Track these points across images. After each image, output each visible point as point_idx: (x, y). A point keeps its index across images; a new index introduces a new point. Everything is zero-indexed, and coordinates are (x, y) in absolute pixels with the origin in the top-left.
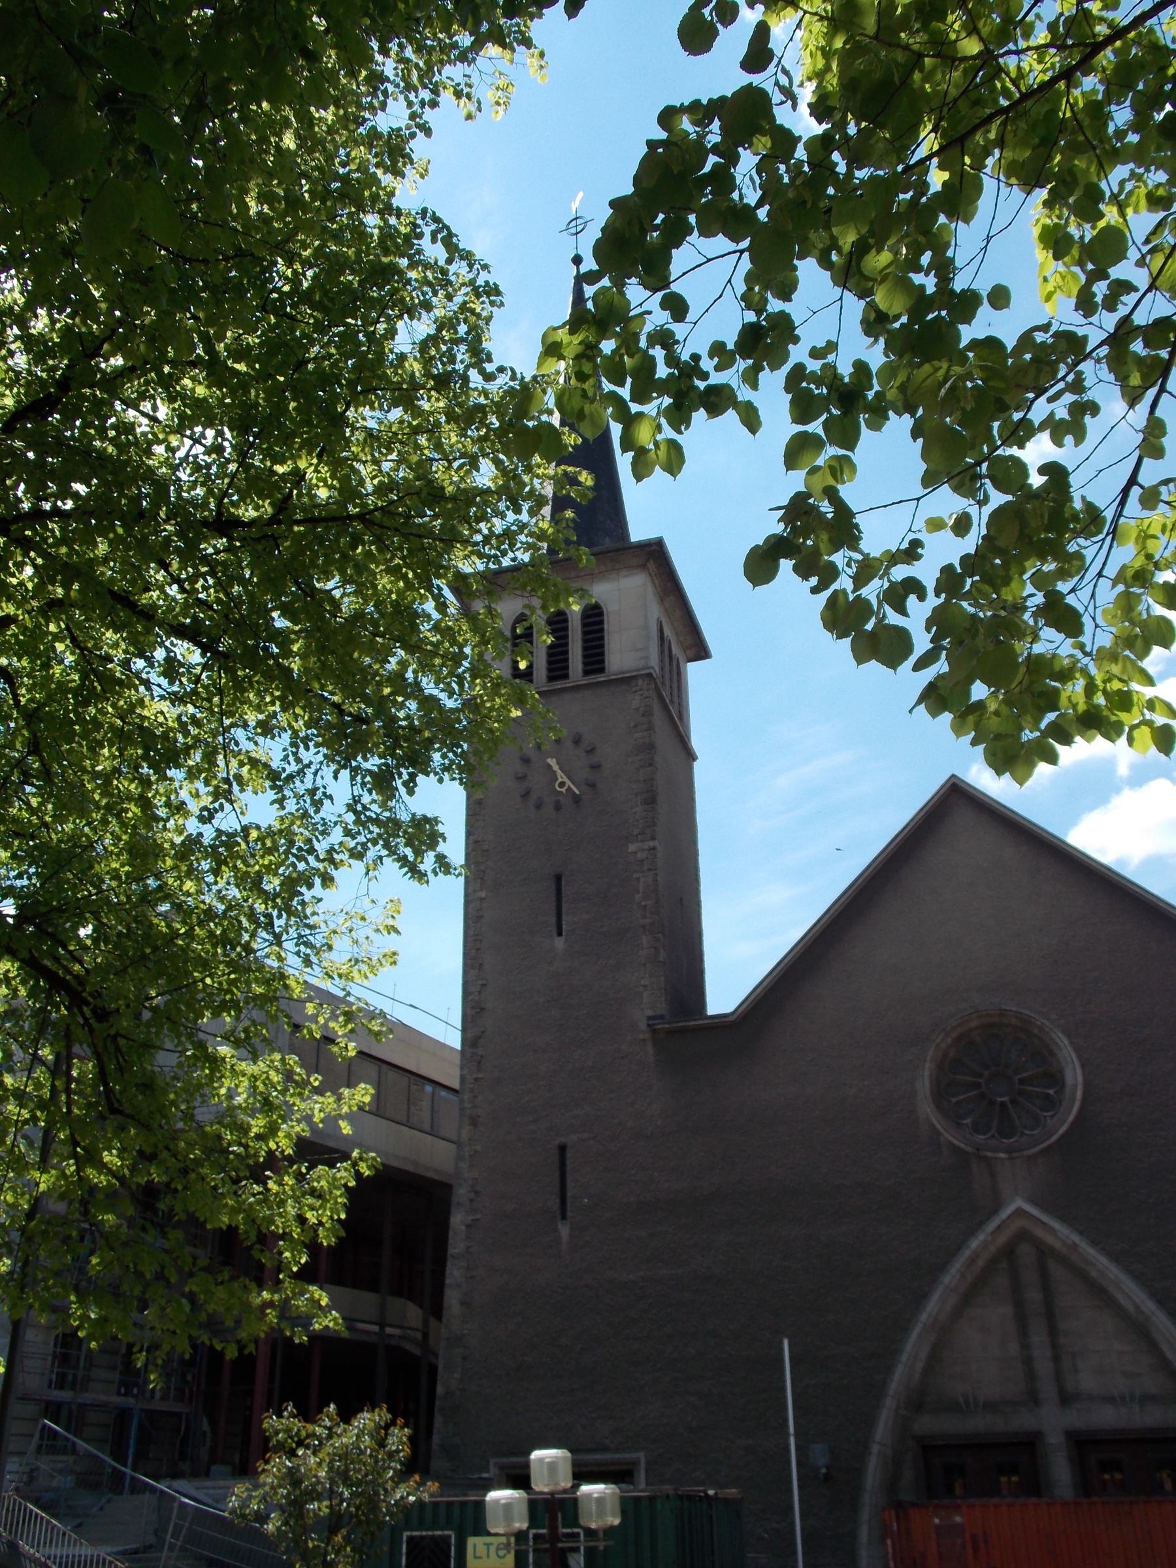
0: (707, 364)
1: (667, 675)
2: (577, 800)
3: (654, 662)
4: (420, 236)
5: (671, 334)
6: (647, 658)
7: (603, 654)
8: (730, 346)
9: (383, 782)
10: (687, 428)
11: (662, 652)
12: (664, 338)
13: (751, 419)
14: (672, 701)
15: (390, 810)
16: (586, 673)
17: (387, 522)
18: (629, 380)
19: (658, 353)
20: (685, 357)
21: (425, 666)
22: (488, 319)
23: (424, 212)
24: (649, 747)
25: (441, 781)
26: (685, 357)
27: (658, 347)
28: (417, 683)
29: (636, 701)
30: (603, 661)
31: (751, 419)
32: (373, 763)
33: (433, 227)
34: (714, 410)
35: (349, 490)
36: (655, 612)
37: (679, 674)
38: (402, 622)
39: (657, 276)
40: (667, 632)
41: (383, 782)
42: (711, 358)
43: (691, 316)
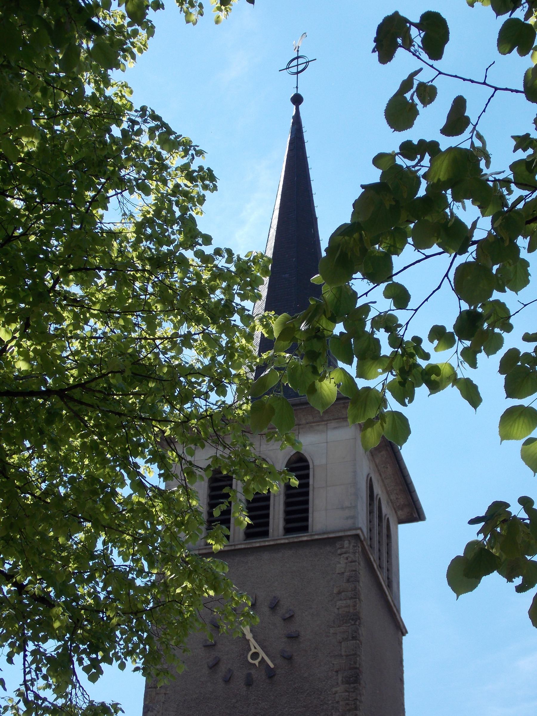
0: (427, 346)
1: (376, 538)
2: (271, 674)
3: (362, 521)
4: (139, 132)
5: (394, 319)
6: (354, 517)
7: (307, 511)
8: (450, 329)
9: (60, 669)
10: (411, 401)
11: (371, 512)
12: (387, 322)
13: (471, 394)
14: (380, 567)
15: (66, 697)
16: (288, 531)
17: (87, 399)
18: (355, 360)
19: (382, 336)
20: (408, 338)
21: (114, 540)
22: (201, 200)
23: (144, 109)
24: (354, 618)
25: (122, 666)
26: (408, 338)
27: (382, 330)
28: (105, 556)
29: (341, 565)
30: (306, 519)
31: (471, 394)
32: (51, 646)
33: (153, 124)
34: (435, 387)
35: (47, 363)
36: (365, 467)
37: (389, 536)
38: (92, 502)
39: (380, 271)
40: (378, 490)
41: (60, 669)
42: (431, 340)
43: (412, 304)
